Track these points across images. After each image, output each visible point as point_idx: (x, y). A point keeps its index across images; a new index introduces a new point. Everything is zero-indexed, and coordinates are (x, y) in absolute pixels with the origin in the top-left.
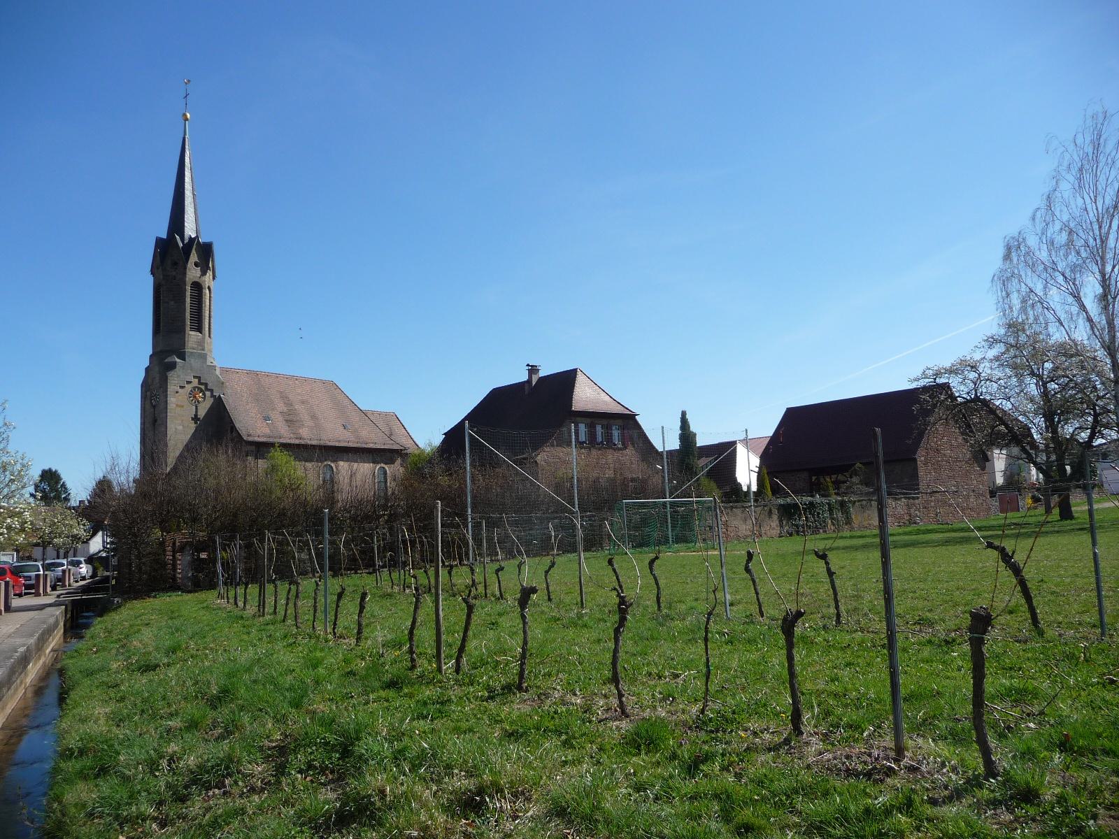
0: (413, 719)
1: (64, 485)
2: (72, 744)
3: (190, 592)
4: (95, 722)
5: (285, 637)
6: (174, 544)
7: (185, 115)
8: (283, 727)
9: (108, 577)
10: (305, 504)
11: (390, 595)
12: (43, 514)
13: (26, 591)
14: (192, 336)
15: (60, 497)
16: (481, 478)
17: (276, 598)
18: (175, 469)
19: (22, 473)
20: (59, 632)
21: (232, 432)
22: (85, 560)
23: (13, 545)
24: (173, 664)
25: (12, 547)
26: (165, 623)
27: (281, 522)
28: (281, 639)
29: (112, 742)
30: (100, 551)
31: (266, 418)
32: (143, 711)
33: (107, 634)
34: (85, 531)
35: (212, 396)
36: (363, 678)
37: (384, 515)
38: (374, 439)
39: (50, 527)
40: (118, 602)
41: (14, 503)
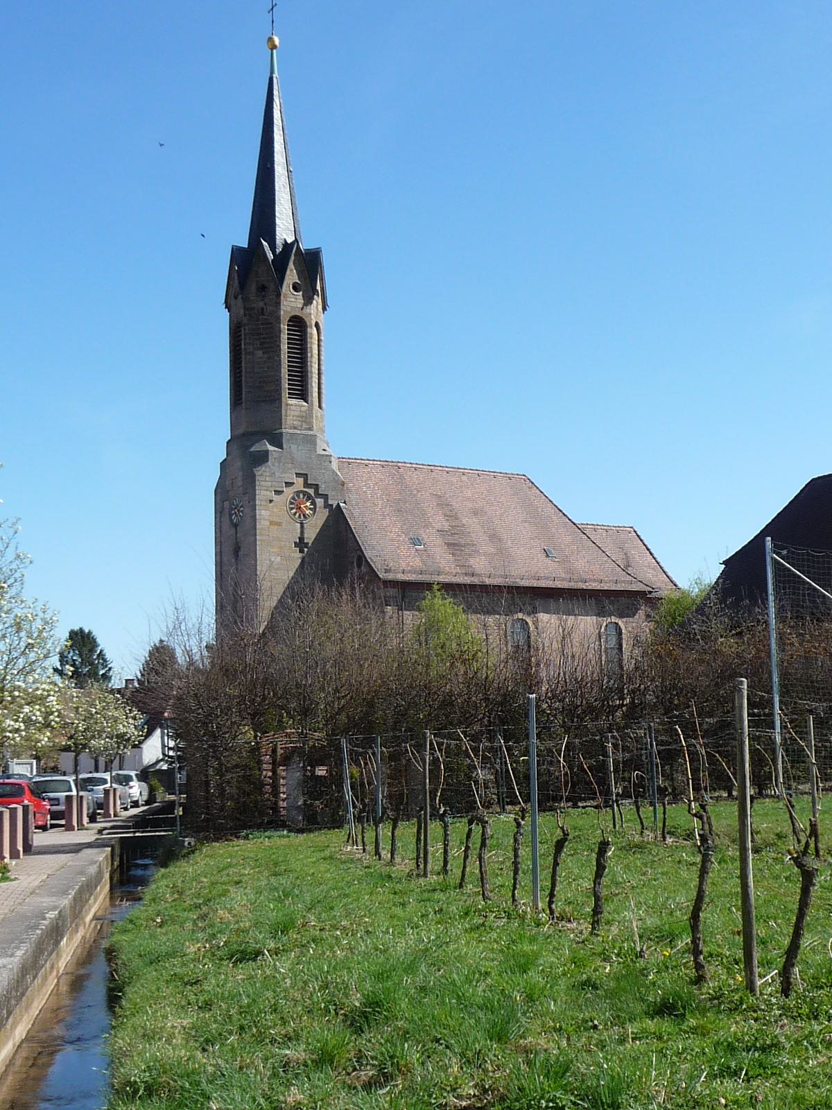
0: (712, 1076)
1: (101, 655)
2: (135, 1076)
3: (301, 831)
4: (169, 1041)
5: (467, 914)
6: (274, 751)
7: (270, 40)
8: (479, 1074)
9: (173, 802)
10: (485, 685)
11: (640, 847)
12: (75, 699)
13: (53, 822)
14: (292, 407)
15: (97, 674)
16: (795, 640)
17: (446, 845)
18: (271, 627)
19: (45, 634)
20: (104, 889)
21: (359, 566)
22: (136, 775)
23: (30, 749)
24: (283, 950)
25: (29, 753)
26: (266, 882)
27: (447, 717)
28: (460, 917)
29: (197, 1078)
30: (158, 762)
31: (416, 541)
32: (242, 1028)
33: (176, 896)
34: (136, 727)
35: (327, 505)
36: (611, 994)
37: (623, 705)
38: (602, 576)
39: (84, 721)
40: (189, 843)
41: (34, 682)
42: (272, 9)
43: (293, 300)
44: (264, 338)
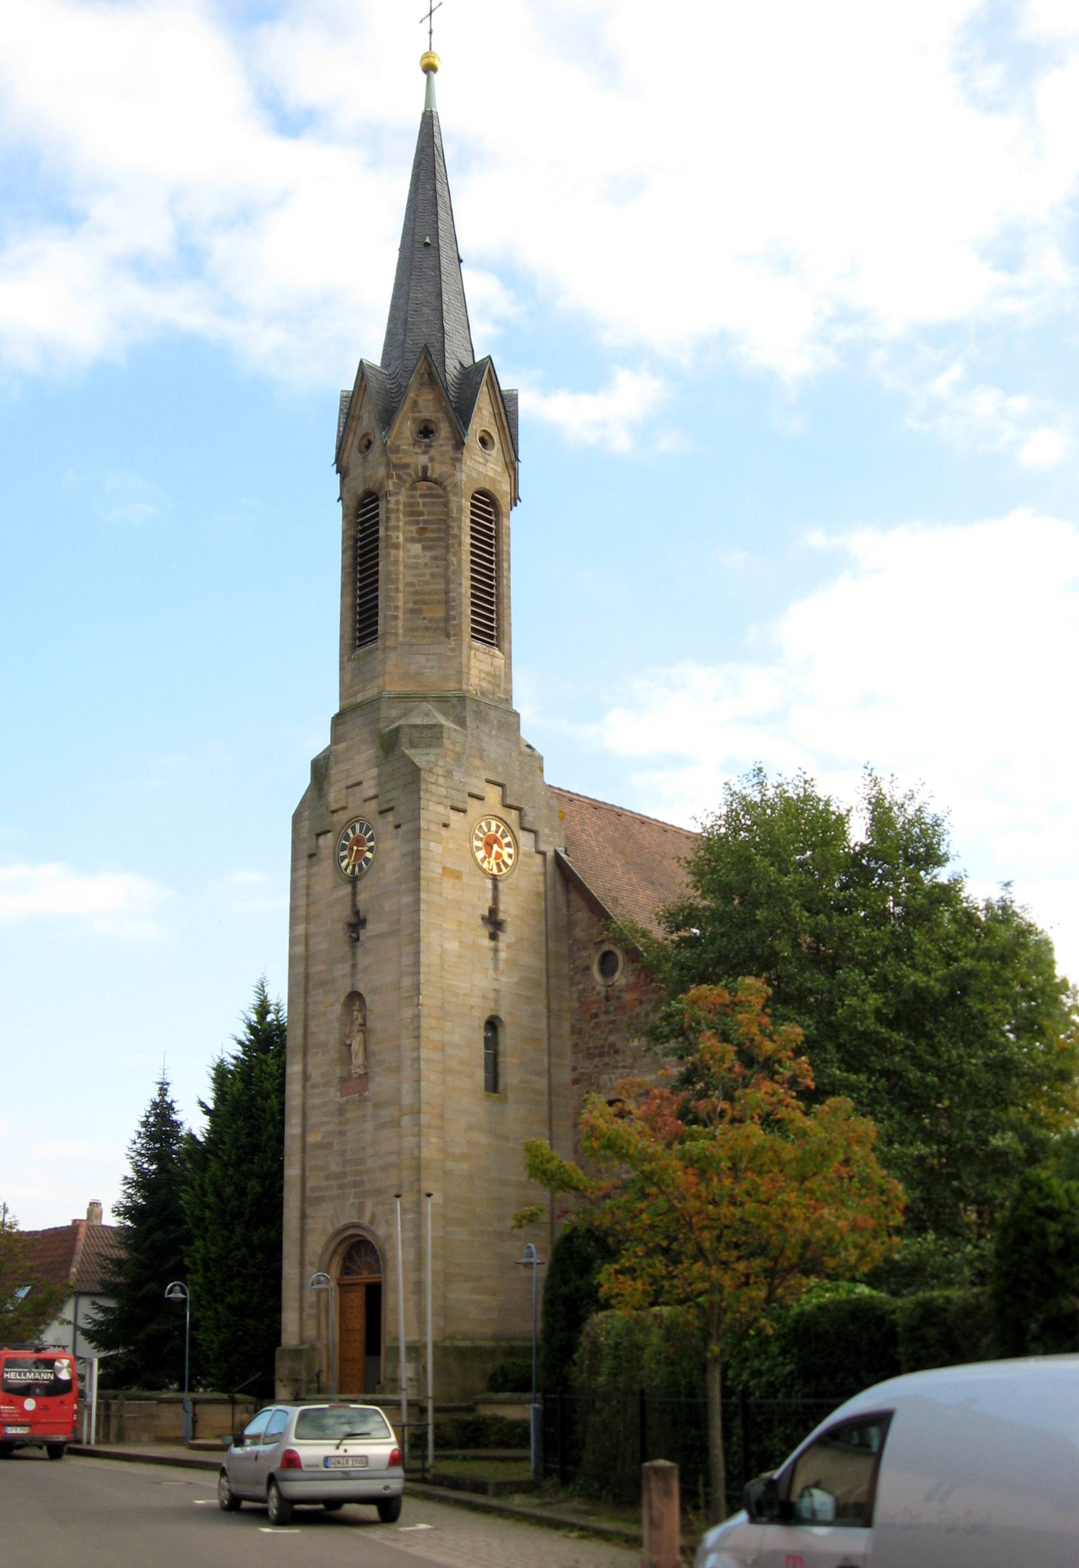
42: (431, 12)
43: (481, 460)
44: (425, 522)
